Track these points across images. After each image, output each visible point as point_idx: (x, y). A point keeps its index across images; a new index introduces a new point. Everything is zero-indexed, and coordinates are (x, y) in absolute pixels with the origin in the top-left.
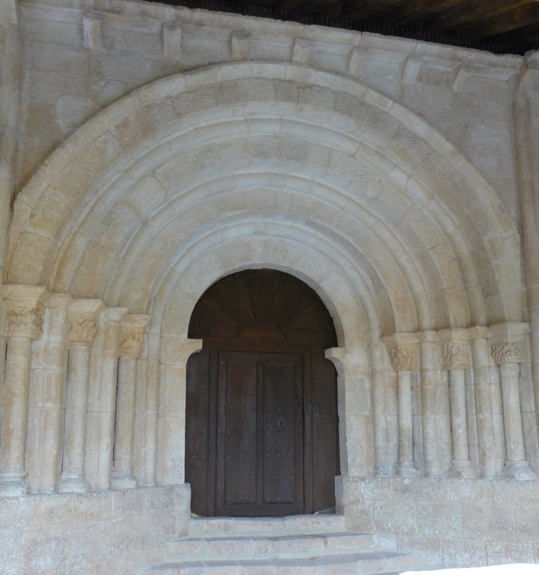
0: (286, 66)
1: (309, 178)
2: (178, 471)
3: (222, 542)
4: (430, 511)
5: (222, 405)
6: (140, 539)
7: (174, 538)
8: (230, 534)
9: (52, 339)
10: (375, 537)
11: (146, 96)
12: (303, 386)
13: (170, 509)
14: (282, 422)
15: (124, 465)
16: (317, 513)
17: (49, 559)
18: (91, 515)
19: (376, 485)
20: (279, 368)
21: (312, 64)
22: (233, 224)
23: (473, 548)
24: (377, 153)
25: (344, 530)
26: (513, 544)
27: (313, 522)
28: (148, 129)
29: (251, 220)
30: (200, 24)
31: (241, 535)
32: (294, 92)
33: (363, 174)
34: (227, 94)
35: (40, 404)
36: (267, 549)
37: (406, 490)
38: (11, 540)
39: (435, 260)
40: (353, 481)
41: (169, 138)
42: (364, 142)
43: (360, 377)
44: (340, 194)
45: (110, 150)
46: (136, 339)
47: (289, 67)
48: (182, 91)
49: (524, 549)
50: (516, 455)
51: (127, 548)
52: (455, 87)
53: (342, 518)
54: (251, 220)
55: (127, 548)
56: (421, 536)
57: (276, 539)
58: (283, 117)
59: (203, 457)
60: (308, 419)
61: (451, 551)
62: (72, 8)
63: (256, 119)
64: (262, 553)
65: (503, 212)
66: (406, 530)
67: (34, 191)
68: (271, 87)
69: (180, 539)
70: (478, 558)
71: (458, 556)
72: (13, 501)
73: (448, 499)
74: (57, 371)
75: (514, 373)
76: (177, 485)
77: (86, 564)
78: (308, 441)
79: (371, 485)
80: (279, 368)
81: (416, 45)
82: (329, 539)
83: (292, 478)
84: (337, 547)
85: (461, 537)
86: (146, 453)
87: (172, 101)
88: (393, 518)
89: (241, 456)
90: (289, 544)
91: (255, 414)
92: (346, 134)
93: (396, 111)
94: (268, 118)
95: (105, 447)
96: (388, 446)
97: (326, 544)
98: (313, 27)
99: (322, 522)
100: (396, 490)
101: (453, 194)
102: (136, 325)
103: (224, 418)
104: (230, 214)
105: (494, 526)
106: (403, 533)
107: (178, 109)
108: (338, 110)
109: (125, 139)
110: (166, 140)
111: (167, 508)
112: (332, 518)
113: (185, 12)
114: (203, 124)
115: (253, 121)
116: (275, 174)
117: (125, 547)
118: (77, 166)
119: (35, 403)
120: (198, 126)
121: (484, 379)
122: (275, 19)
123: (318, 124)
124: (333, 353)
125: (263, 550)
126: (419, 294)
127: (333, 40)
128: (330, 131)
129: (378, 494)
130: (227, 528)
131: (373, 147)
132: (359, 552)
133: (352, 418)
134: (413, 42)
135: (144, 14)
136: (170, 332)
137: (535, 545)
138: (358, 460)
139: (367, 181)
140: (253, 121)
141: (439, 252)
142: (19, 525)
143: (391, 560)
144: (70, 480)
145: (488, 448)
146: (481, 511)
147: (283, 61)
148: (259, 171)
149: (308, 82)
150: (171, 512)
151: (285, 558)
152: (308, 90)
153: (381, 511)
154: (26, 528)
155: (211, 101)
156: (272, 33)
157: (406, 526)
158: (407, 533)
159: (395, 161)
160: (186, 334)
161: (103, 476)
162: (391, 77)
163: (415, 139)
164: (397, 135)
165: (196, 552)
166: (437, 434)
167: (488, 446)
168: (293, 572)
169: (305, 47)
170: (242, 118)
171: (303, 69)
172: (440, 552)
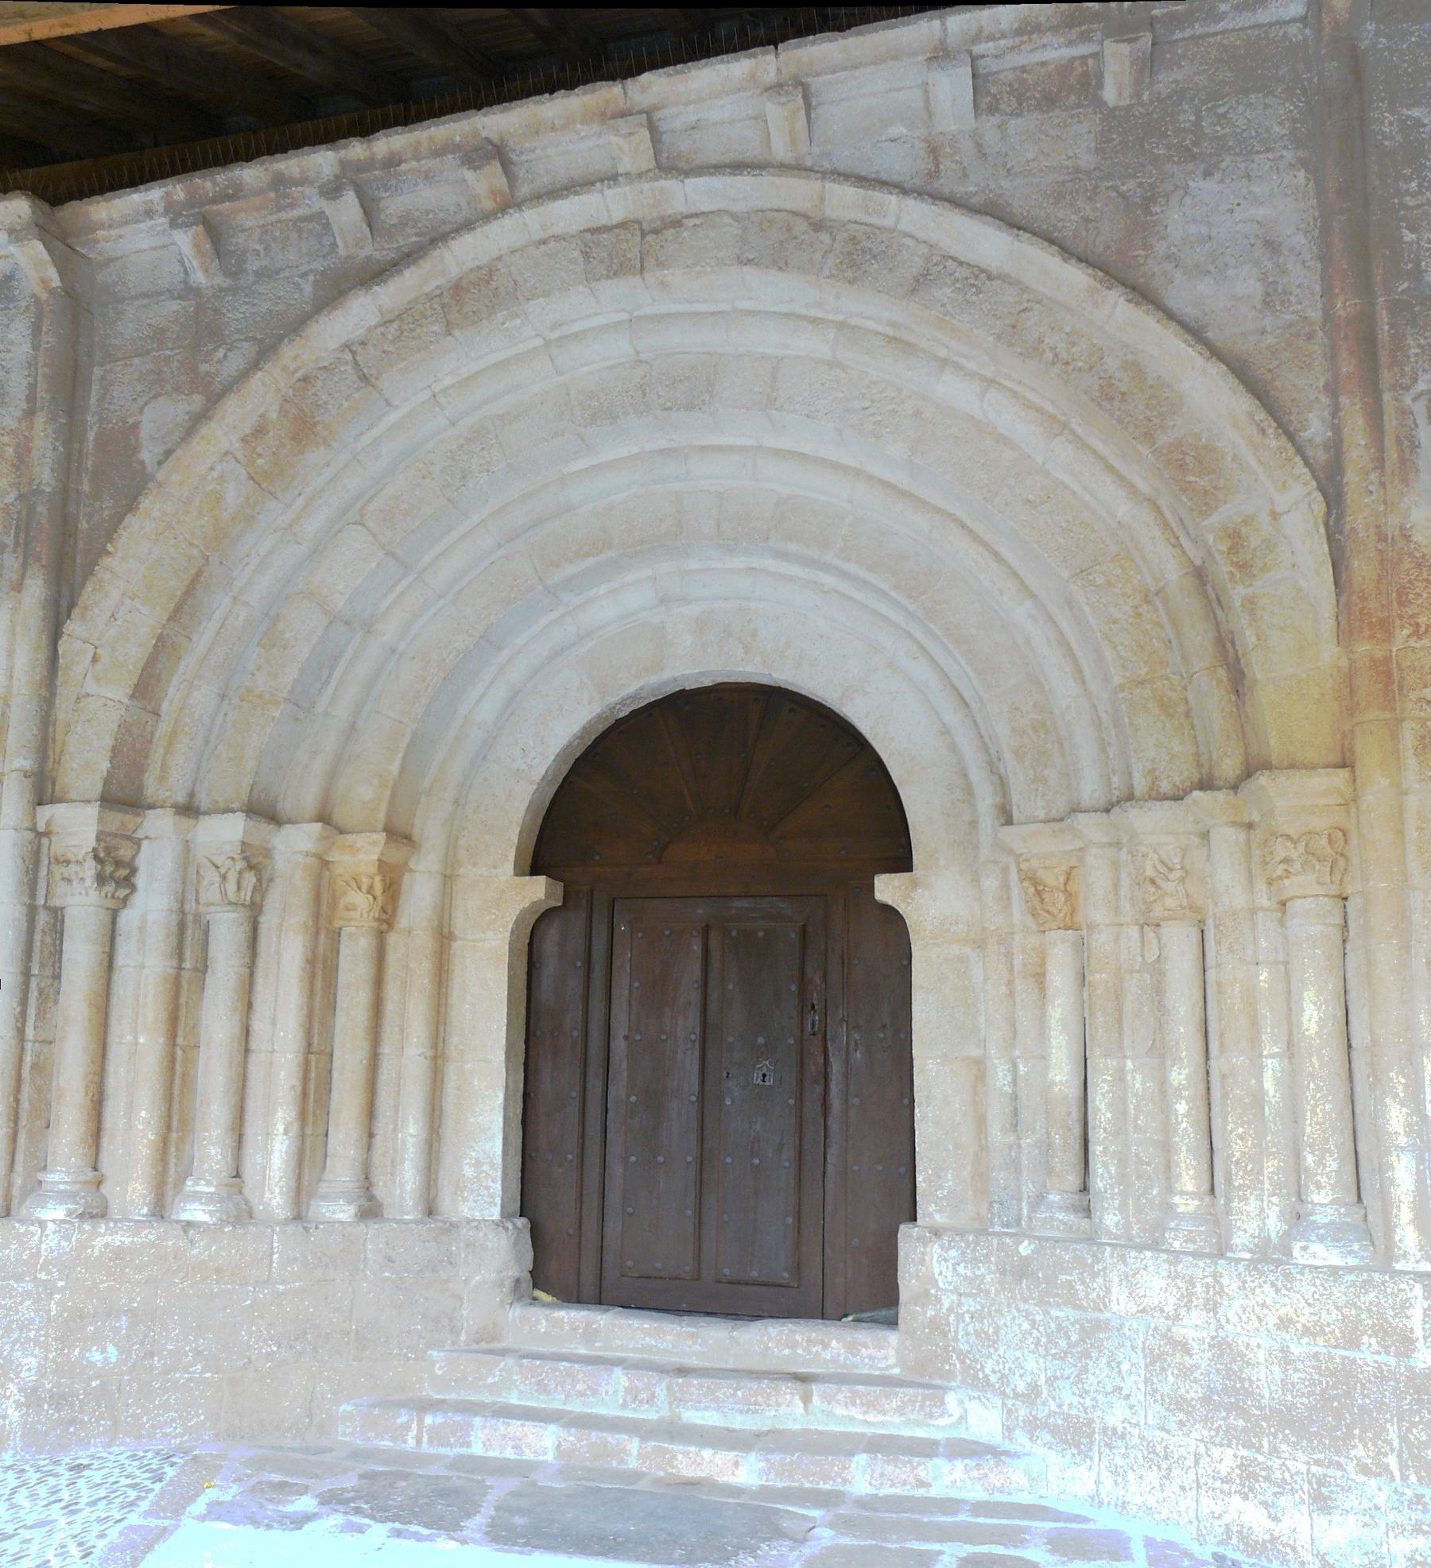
0: (602, 192)
1: (749, 442)
2: (487, 1188)
3: (549, 1365)
4: (1074, 1337)
5: (620, 1030)
6: (352, 1335)
7: (454, 1343)
8: (598, 1349)
9: (151, 904)
10: (951, 1399)
11: (296, 357)
12: (825, 977)
13: (443, 1275)
14: (764, 1076)
15: (342, 1167)
16: (850, 1318)
17: (112, 1350)
18: (218, 1271)
19: (963, 1253)
20: (761, 934)
21: (669, 165)
22: (603, 589)
23: (1166, 1458)
24: (892, 340)
25: (896, 1371)
26: (1261, 1459)
27: (809, 1340)
28: (303, 426)
29: (648, 572)
30: (392, 162)
31: (624, 1355)
32: (627, 250)
33: (868, 404)
34: (470, 300)
35: (129, 1037)
36: (653, 1396)
37: (1021, 1271)
38: (27, 1303)
39: (1087, 609)
40: (918, 1239)
41: (374, 433)
42: (852, 321)
43: (956, 950)
44: (835, 466)
45: (233, 495)
46: (364, 888)
47: (608, 193)
48: (373, 323)
49: (1287, 1476)
50: (1319, 1186)
51: (315, 1350)
52: (1109, 95)
53: (893, 1337)
54: (648, 572)
55: (315, 1350)
56: (1053, 1406)
57: (682, 1371)
58: (636, 313)
59: (570, 1157)
60: (836, 1067)
61: (1119, 1461)
62: (151, 218)
63: (566, 337)
64: (641, 1402)
65: (1263, 431)
66: (1021, 1388)
67: (96, 611)
68: (576, 254)
69: (475, 1346)
70: (1176, 1489)
71: (1131, 1475)
72: (31, 1228)
73: (1114, 1306)
74: (158, 970)
75: (1316, 929)
76: (469, 1221)
77: (202, 1372)
78: (834, 1125)
79: (953, 1253)
80: (761, 934)
81: (943, 24)
82: (815, 1388)
83: (790, 1220)
84: (840, 1411)
85: (1142, 1422)
86: (404, 1143)
87: (354, 353)
88: (996, 1350)
89: (660, 1159)
90: (708, 1388)
91: (697, 1054)
92: (804, 312)
93: (914, 217)
94: (591, 328)
95: (281, 1128)
96: (1019, 1146)
97: (806, 1399)
98: (646, 77)
99: (834, 1343)
100: (1003, 1273)
101: (1126, 401)
102: (361, 856)
103: (624, 1065)
104: (571, 570)
105: (1216, 1397)
106: (1016, 1396)
107: (362, 368)
108: (749, 262)
109: (260, 461)
110: (367, 438)
111: (434, 1270)
112: (865, 1336)
113: (356, 149)
114: (449, 381)
115: (561, 341)
116: (661, 452)
117: (309, 1348)
118: (172, 542)
119: (121, 1037)
120: (437, 388)
121: (1231, 950)
122: (551, 93)
123: (726, 307)
124: (887, 888)
125: (644, 1396)
126: (1069, 707)
127: (715, 95)
128: (769, 316)
129: (966, 1278)
130: (590, 1335)
131: (880, 329)
132: (594, 1411)
133: (931, 1065)
134: (931, 19)
135: (280, 182)
136: (474, 865)
137: (1314, 1469)
138: (949, 1181)
139: (879, 423)
140: (561, 341)
141: (1100, 580)
142: (42, 1276)
143: (959, 1465)
144: (196, 1197)
145: (1237, 1162)
146: (1186, 1350)
147: (592, 184)
148: (622, 451)
149: (670, 212)
150: (447, 1281)
151: (698, 1421)
152: (670, 233)
153: (970, 1329)
154: (61, 1284)
155: (435, 328)
156: (557, 128)
157: (1021, 1376)
158: (1023, 1395)
159: (943, 353)
160: (509, 867)
161: (277, 1190)
162: (899, 130)
163: (978, 278)
164: (920, 283)
165: (490, 1380)
166: (1125, 1113)
167: (1238, 1154)
168: (680, 1457)
169: (631, 134)
170: (539, 342)
171: (646, 186)
172: (1092, 1459)
